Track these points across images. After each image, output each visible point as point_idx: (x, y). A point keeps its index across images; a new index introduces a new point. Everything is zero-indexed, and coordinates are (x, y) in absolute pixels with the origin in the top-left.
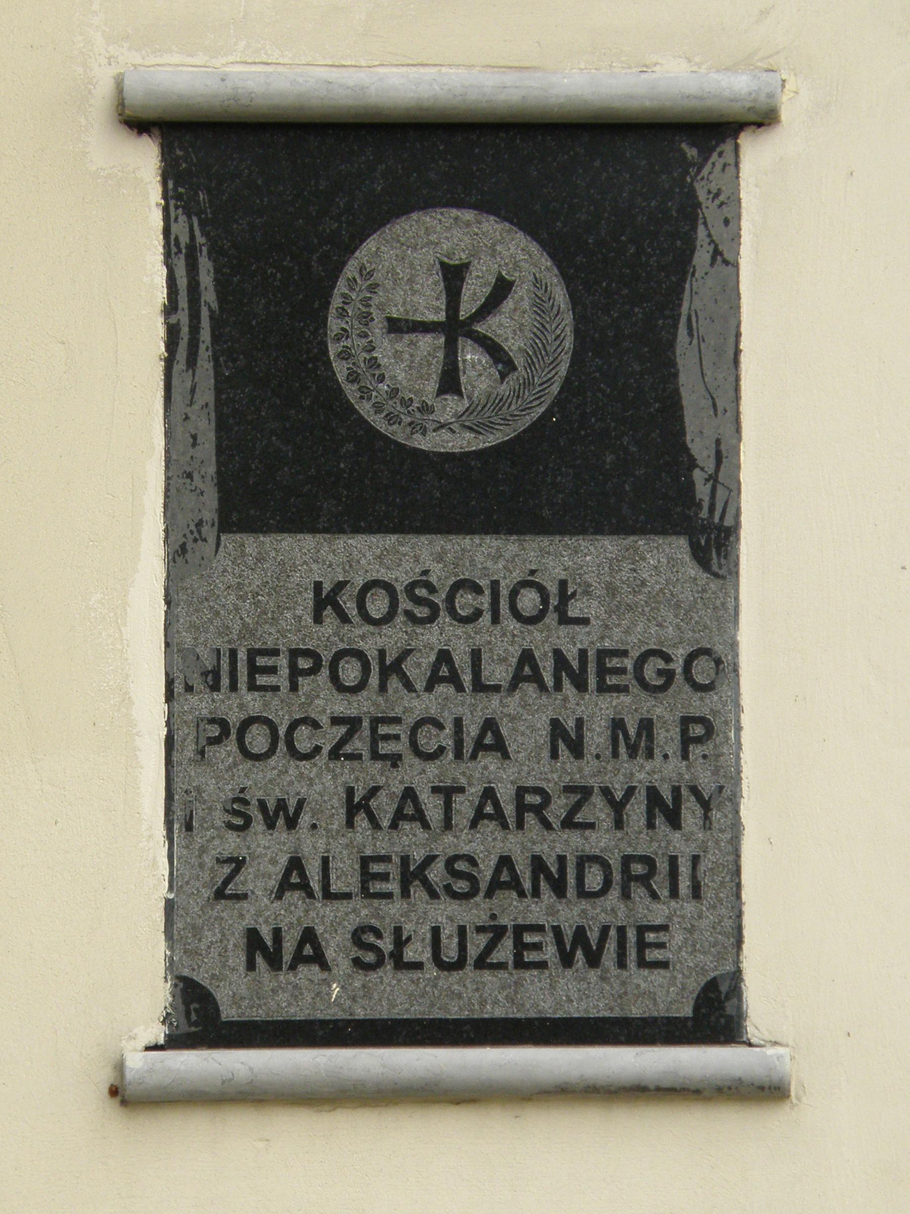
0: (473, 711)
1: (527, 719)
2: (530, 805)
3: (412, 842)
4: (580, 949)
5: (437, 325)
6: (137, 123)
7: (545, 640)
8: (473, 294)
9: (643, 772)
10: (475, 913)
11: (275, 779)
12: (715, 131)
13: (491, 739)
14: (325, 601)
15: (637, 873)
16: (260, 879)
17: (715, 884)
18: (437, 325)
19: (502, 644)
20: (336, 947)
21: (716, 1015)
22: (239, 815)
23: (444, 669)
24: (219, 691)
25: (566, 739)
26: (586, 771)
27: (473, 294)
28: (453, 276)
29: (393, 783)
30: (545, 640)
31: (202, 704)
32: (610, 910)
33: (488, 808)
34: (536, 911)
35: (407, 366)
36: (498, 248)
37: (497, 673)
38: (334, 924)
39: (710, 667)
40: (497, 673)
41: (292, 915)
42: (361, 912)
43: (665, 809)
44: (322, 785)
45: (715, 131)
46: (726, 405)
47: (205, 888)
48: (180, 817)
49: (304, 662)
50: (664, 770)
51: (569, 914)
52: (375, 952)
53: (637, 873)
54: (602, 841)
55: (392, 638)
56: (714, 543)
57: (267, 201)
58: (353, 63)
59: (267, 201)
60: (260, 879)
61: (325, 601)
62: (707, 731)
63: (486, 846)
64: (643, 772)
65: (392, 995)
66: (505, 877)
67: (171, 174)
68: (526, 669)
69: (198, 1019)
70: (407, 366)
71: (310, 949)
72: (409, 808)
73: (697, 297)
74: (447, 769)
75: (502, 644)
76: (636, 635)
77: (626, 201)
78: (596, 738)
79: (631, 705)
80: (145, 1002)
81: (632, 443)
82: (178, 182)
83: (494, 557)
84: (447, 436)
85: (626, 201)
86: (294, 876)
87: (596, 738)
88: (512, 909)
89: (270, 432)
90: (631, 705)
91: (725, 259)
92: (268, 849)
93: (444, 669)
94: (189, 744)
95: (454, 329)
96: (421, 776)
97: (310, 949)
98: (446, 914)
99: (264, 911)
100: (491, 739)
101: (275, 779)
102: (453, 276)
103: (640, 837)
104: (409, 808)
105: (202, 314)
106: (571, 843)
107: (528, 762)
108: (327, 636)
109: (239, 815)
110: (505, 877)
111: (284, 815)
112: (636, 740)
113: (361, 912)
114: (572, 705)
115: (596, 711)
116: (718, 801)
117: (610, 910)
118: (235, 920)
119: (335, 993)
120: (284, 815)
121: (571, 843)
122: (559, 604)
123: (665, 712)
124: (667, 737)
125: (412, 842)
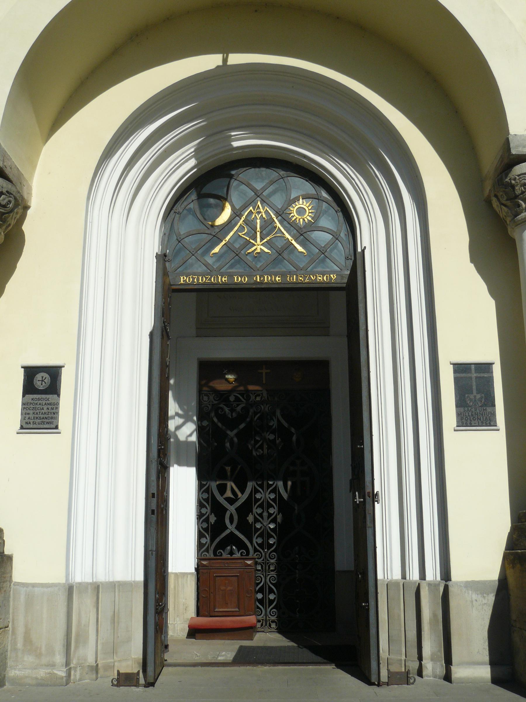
0: (42, 407)
1: (45, 407)
2: (45, 413)
3: (37, 416)
4: (48, 423)
5: (41, 381)
6: (22, 367)
7: (47, 402)
8: (44, 378)
9: (53, 411)
10: (41, 421)
11: (28, 411)
12: (61, 367)
13: (43, 409)
14: (32, 399)
15: (52, 418)
16: (27, 418)
17: (57, 418)
18: (41, 381)
19: (44, 402)
20: (31, 423)
21: (57, 427)
22: (26, 414)
23: (40, 404)
25: (48, 409)
26: (49, 411)
27: (44, 378)
28: (42, 377)
29: (36, 412)
30: (47, 402)
31: (24, 406)
32: (50, 420)
33: (42, 414)
34: (45, 420)
35: (39, 383)
36: (45, 375)
37: (43, 404)
38: (31, 421)
39: (58, 404)
40: (43, 404)
41: (29, 421)
42: (33, 420)
43: (54, 413)
44: (31, 412)
45: (61, 367)
46: (60, 386)
47: (23, 418)
48: (22, 414)
49: (31, 403)
50: (54, 411)
51: (47, 421)
52: (34, 423)
53: (52, 418)
54: (50, 416)
55: (37, 402)
56: (59, 395)
57: (30, 372)
58: (98, 658)
59: (30, 372)
60: (27, 418)
61: (32, 399)
62: (57, 408)
63: (42, 416)
64: (53, 411)
65: (35, 426)
66: (43, 418)
67: (24, 371)
68: (45, 404)
69: (22, 428)
70: (39, 383)
71: (30, 423)
72: (37, 413)
73: (160, 303)
74: (40, 411)
75: (44, 402)
76: (53, 402)
77: (54, 373)
78: (50, 409)
79: (52, 406)
80: (19, 426)
81: (54, 388)
82: (25, 372)
83: (44, 396)
84: (41, 388)
85: (54, 373)
86: (29, 418)
87: (50, 409)
88: (43, 420)
89: (29, 388)
90: (52, 406)
91: (61, 376)
92: (27, 416)
93: (40, 404)
94: (23, 409)
95: (42, 381)
96: (38, 411)
97: (30, 423)
98: (39, 421)
99: (27, 420)
100: (43, 409)
101: (28, 411)
102: (42, 377)
103: (52, 415)
104: (37, 413)
105: (220, 501)
106: (48, 416)
107: (45, 410)
108: (32, 402)
109: (26, 414)
110: (43, 418)
111: (29, 414)
112: (52, 409)
113: (33, 420)
114: (48, 406)
115: (50, 407)
116: (58, 413)
117: (50, 420)
118: (25, 421)
119: (31, 426)
120: (29, 414)
121: (48, 416)
122: (48, 400)
123: (54, 407)
124: (55, 409)
125: (37, 416)
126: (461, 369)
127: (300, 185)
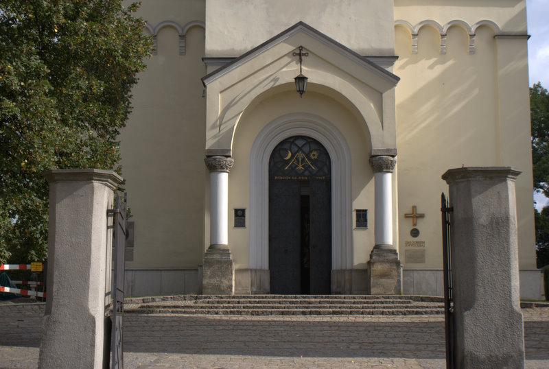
24: (235, 220)
77: (243, 211)
85: (243, 211)
126: (358, 211)
127: (313, 146)
